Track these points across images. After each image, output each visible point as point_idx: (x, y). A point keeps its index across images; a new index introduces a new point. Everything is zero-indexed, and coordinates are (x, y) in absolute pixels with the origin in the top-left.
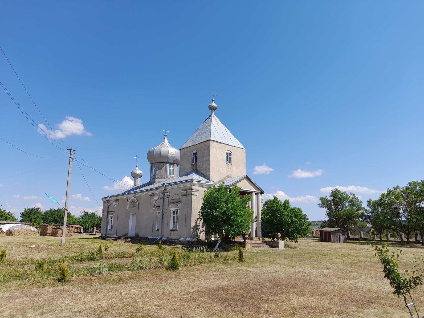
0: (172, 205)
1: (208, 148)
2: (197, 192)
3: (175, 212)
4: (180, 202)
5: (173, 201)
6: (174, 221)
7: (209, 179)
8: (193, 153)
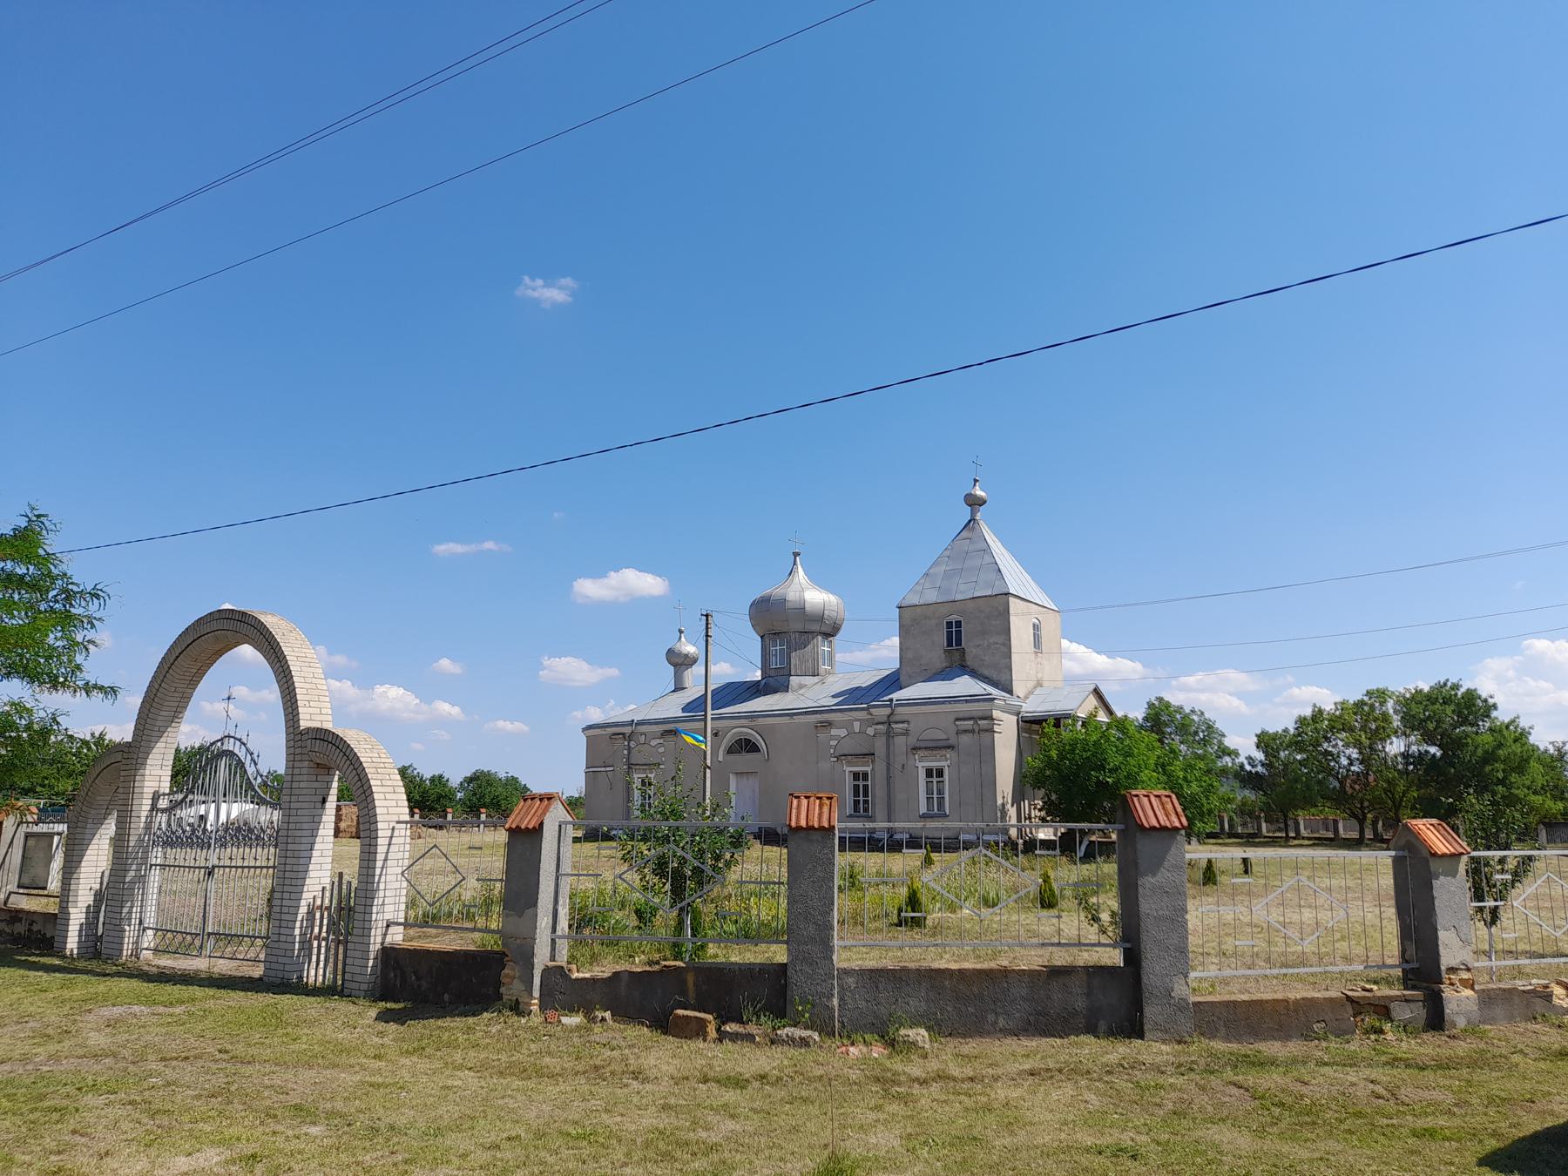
0: (921, 753)
1: (1006, 613)
2: (999, 725)
3: (934, 773)
4: (951, 747)
5: (923, 744)
6: (940, 792)
7: (1010, 692)
8: (947, 623)
